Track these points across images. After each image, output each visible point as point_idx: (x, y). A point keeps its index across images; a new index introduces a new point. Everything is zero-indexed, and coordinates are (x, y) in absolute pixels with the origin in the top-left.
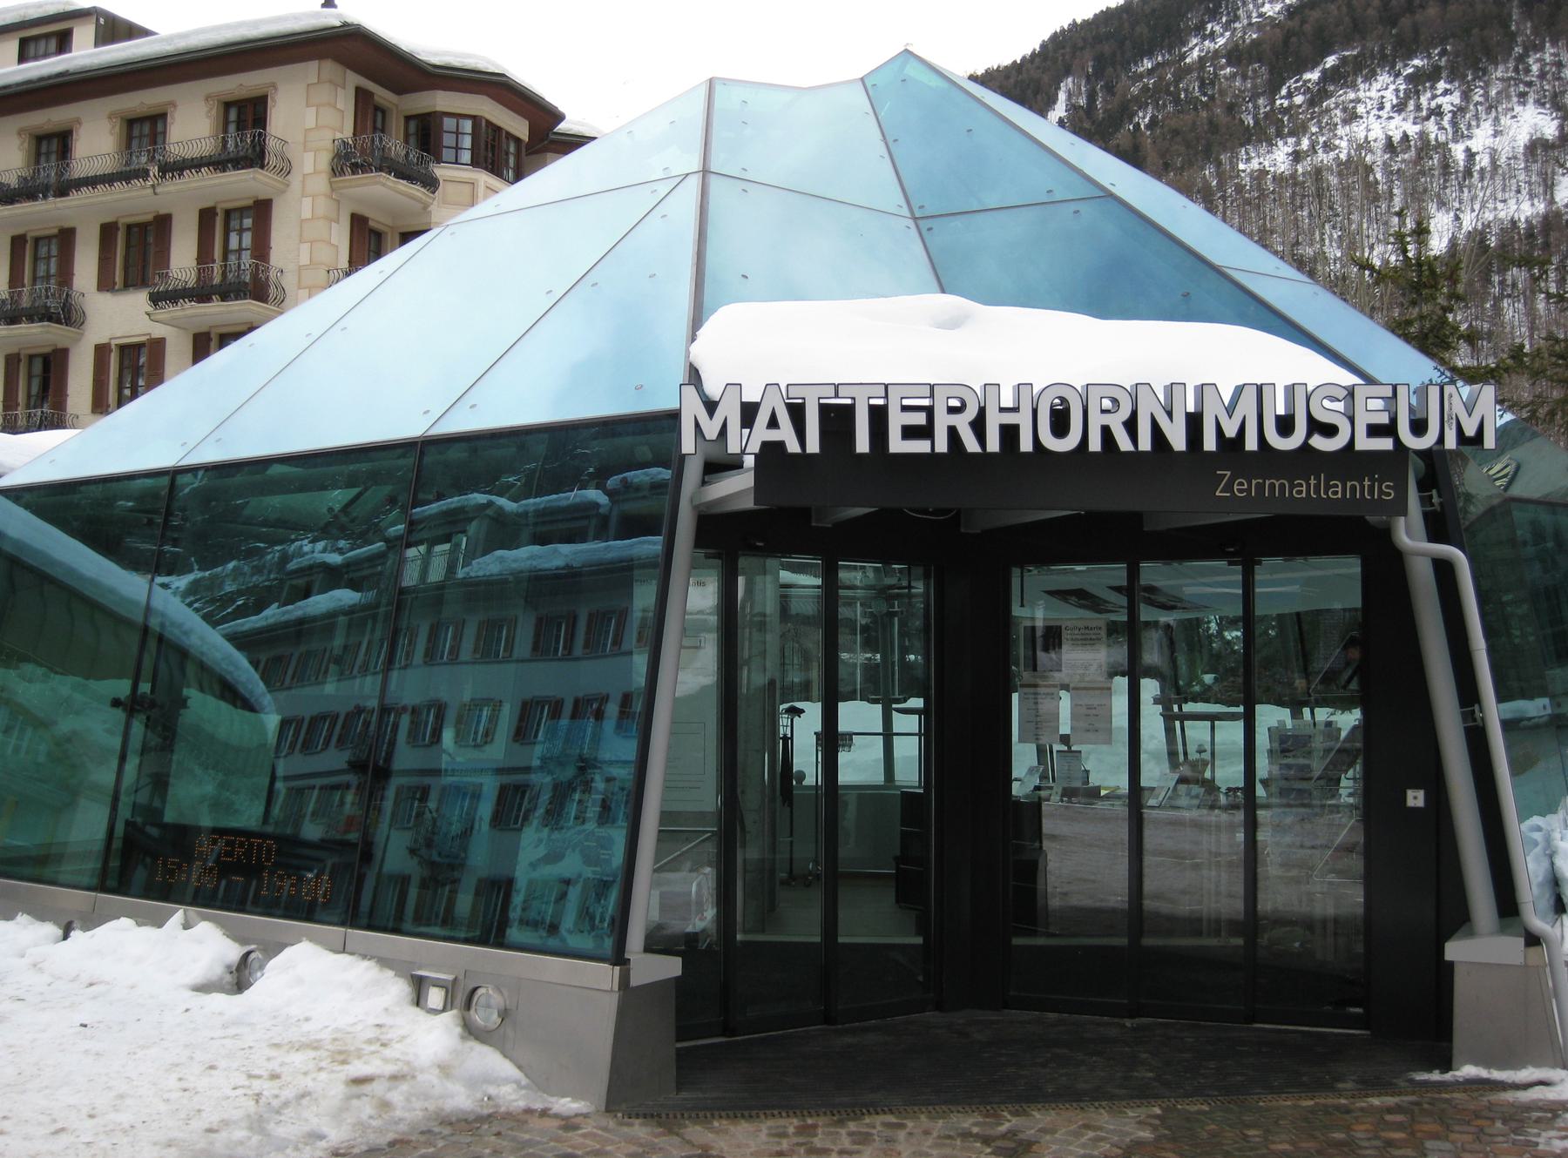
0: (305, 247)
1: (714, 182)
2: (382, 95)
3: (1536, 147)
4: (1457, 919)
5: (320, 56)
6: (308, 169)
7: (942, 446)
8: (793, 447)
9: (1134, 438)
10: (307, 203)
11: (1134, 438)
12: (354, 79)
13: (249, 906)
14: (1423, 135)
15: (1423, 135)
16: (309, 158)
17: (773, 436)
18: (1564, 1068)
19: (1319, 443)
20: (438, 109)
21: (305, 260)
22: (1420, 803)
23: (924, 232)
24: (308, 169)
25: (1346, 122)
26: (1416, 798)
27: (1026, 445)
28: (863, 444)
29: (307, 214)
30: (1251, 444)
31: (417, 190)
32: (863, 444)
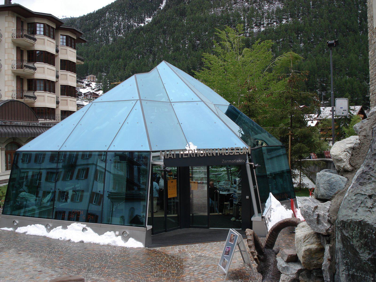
0: (6, 55)
1: (142, 101)
2: (23, 18)
3: (278, 10)
4: (252, 214)
5: (9, 10)
6: (6, 36)
7: (189, 156)
8: (172, 157)
9: (210, 155)
10: (6, 44)
11: (210, 155)
12: (16, 15)
13: (71, 220)
14: (252, 7)
15: (252, 7)
16: (6, 34)
17: (170, 156)
18: (1, 134)
19: (230, 154)
20: (35, 22)
21: (6, 58)
22: (248, 198)
23: (173, 105)
24: (6, 36)
25: (235, 3)
26: (247, 197)
27: (198, 156)
28: (180, 157)
29: (6, 47)
30: (223, 154)
31: (32, 41)
32: (180, 157)
